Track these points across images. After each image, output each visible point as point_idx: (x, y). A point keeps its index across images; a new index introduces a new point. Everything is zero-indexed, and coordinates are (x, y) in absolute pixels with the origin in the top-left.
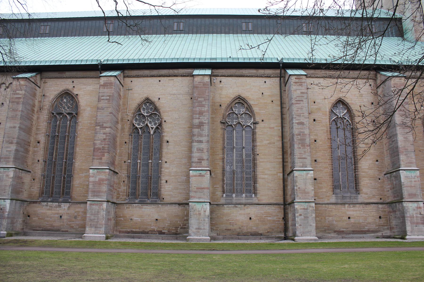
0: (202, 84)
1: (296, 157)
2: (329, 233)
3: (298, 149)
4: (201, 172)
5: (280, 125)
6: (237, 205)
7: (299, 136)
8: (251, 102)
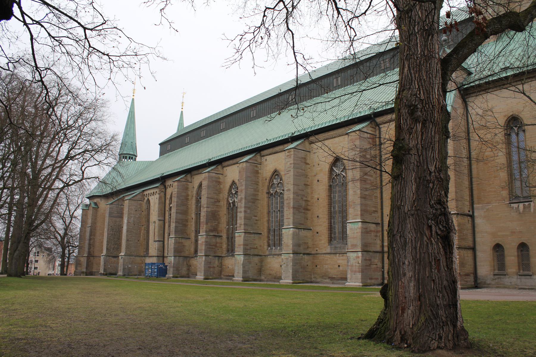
2: (325, 279)
4: (240, 233)
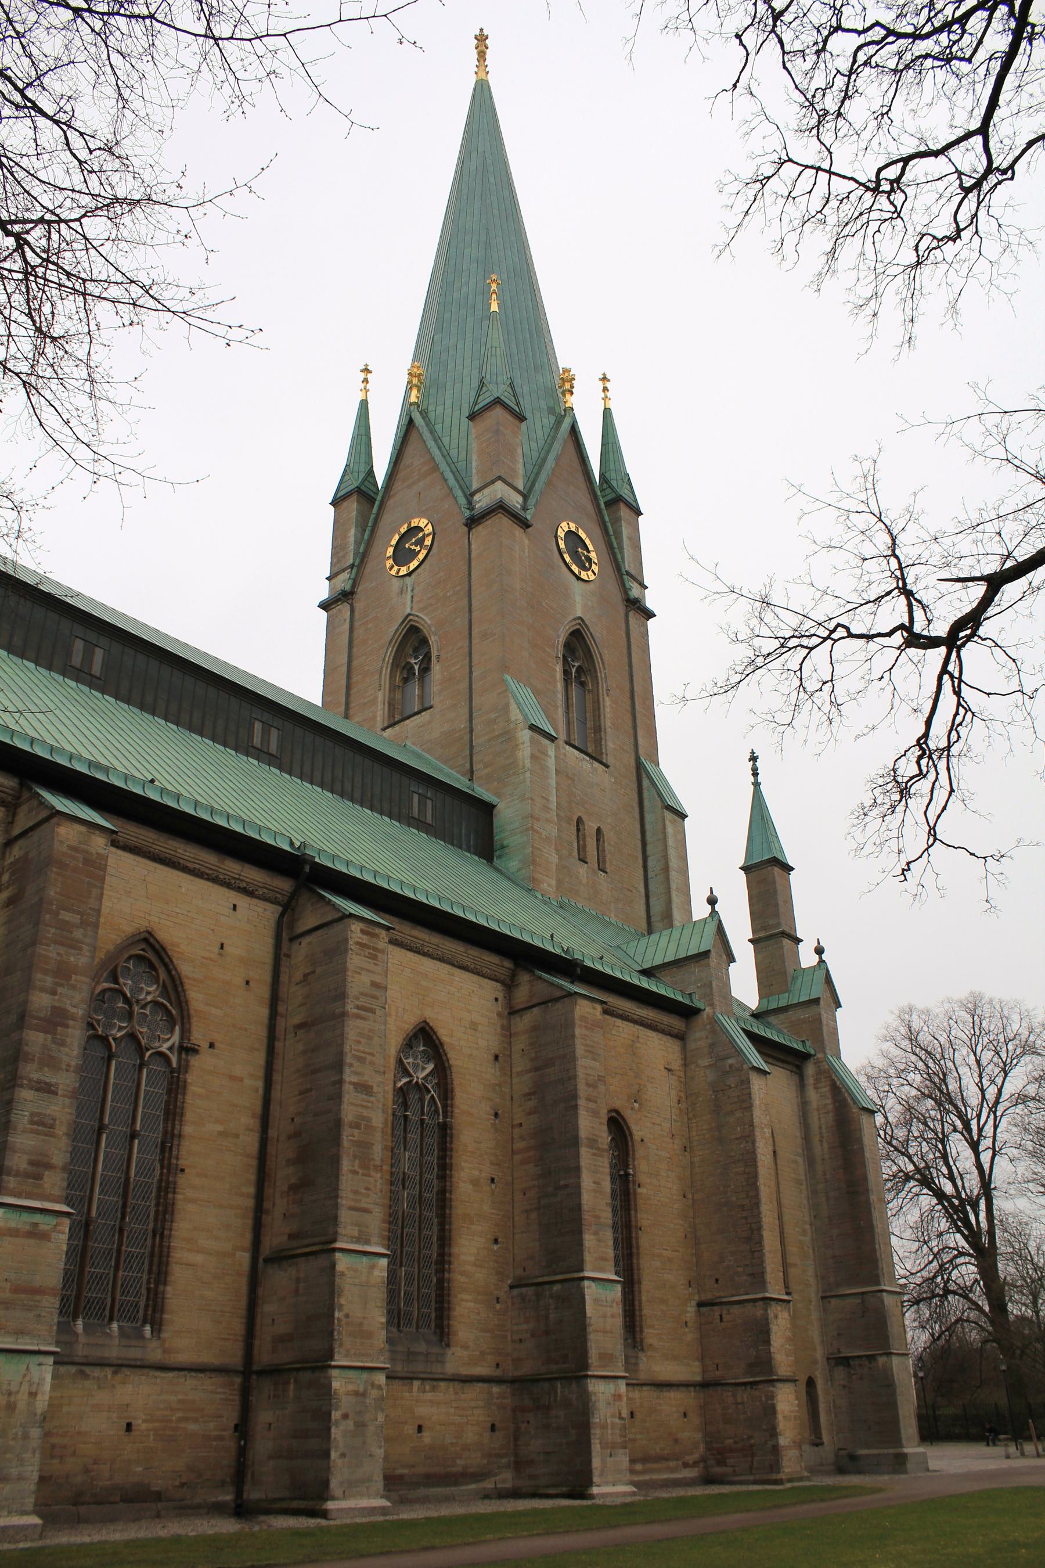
0: (80, 856)
1: (344, 1202)
3: (350, 1176)
4: (37, 1218)
5: (261, 1073)
6: (87, 1370)
7: (356, 1132)
8: (185, 969)
